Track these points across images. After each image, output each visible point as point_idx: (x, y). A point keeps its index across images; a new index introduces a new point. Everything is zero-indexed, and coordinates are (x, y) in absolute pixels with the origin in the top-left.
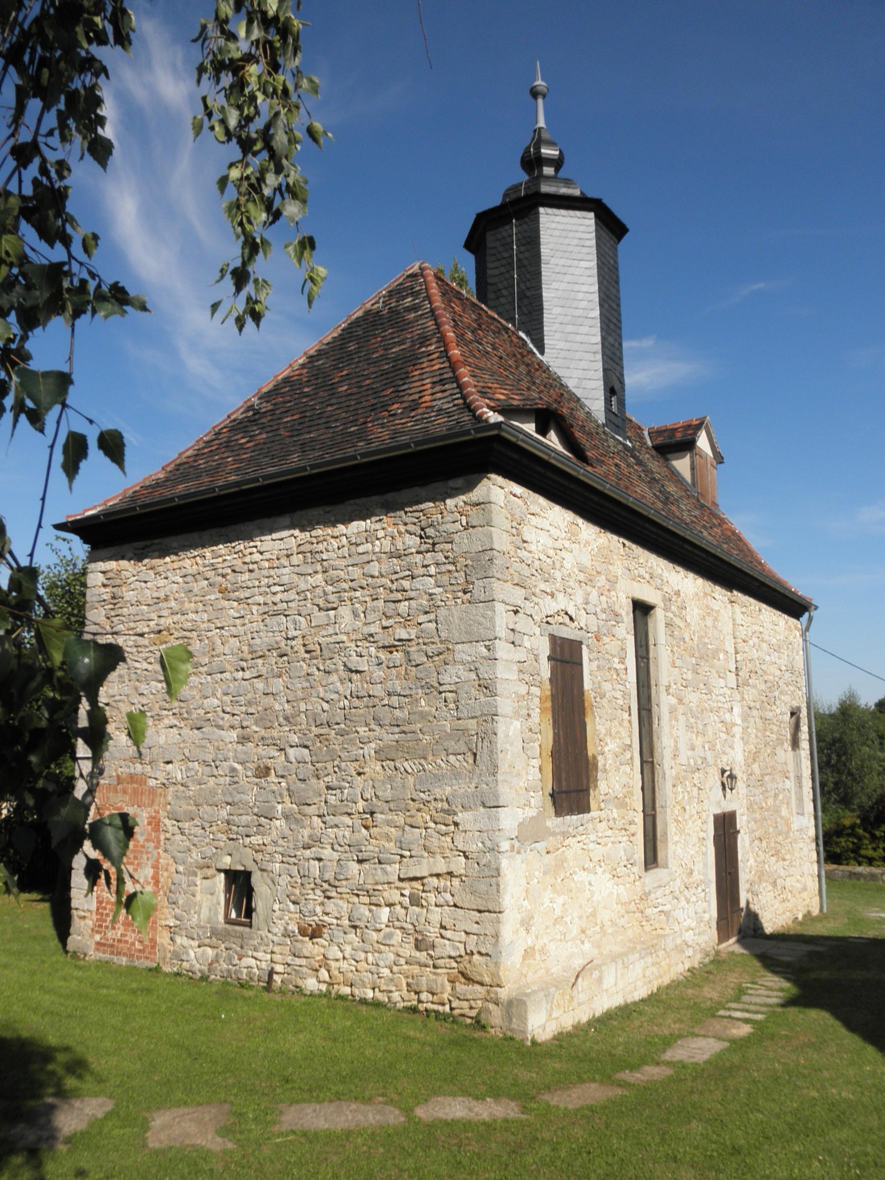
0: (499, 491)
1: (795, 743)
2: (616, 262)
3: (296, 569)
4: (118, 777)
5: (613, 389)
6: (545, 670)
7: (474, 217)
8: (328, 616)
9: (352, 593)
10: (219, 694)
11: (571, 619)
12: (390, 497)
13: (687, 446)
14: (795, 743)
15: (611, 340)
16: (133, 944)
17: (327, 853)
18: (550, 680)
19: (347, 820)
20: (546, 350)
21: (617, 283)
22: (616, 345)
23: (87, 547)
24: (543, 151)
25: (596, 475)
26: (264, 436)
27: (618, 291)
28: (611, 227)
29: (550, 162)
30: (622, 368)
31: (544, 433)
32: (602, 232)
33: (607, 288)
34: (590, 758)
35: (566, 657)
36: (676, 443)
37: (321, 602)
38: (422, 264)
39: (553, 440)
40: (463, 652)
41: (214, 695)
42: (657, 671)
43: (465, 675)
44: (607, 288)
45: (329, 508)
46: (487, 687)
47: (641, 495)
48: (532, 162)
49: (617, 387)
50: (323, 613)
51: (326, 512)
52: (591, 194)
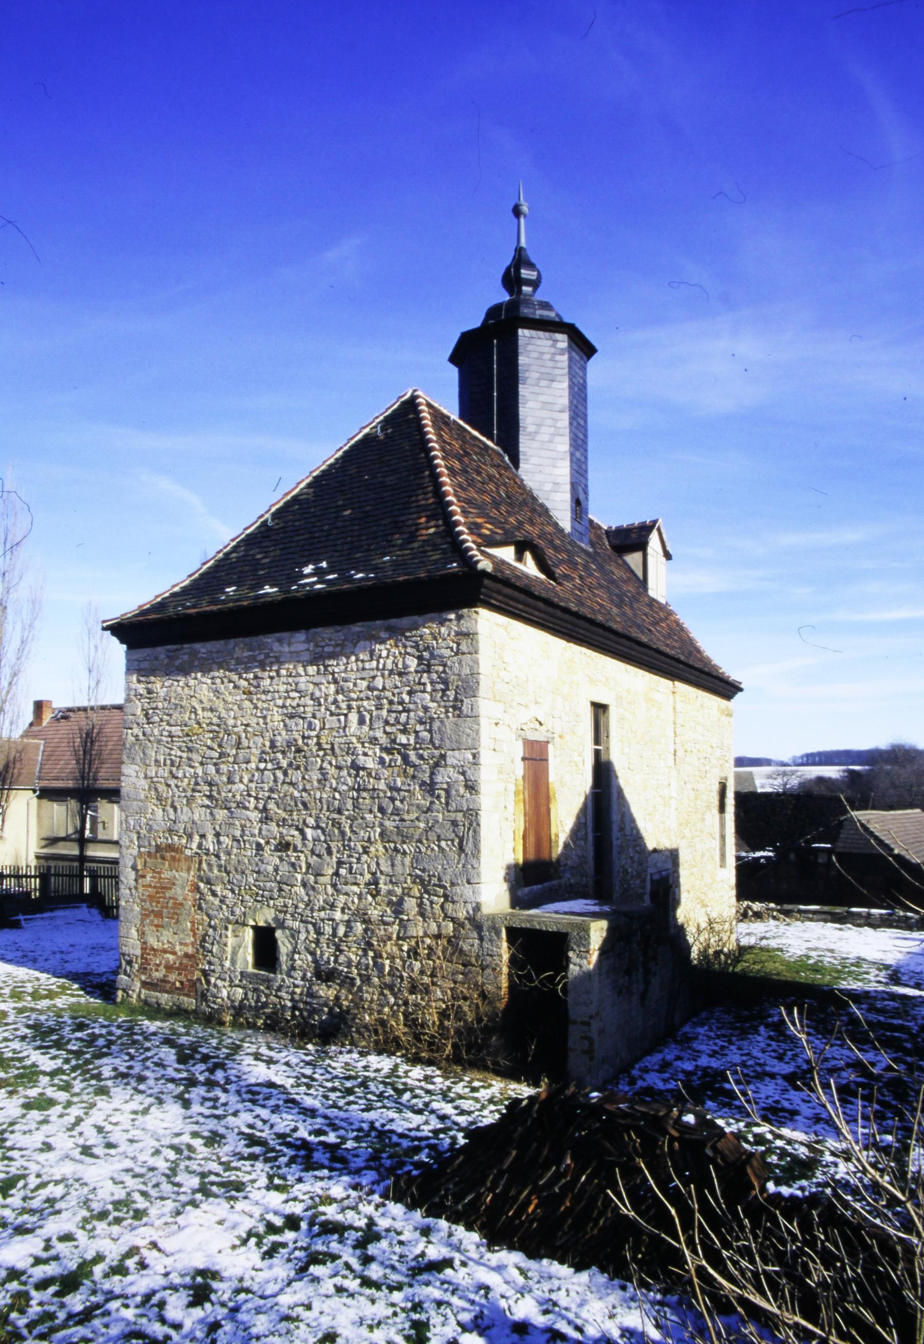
0: (487, 622)
1: (722, 808)
2: (585, 381)
3: (311, 679)
4: (157, 845)
5: (578, 505)
6: (519, 769)
7: (459, 335)
8: (339, 720)
9: (360, 703)
10: (246, 780)
11: (541, 724)
12: (393, 621)
13: (642, 546)
14: (722, 808)
15: (578, 454)
16: (174, 984)
17: (338, 915)
18: (524, 777)
19: (355, 889)
20: (521, 465)
21: (585, 400)
22: (583, 459)
23: (124, 647)
24: (523, 271)
25: (564, 593)
26: (278, 552)
27: (586, 408)
28: (583, 348)
29: (529, 282)
30: (587, 479)
31: (520, 557)
32: (574, 354)
33: (576, 407)
34: (553, 837)
35: (536, 757)
36: (632, 539)
37: (333, 708)
38: (415, 391)
39: (530, 567)
40: (453, 758)
41: (241, 781)
42: (587, 498)
43: (456, 776)
44: (576, 407)
45: (339, 628)
46: (471, 787)
47: (599, 604)
48: (512, 281)
49: (582, 497)
50: (335, 718)
51: (337, 631)
52: (567, 319)
